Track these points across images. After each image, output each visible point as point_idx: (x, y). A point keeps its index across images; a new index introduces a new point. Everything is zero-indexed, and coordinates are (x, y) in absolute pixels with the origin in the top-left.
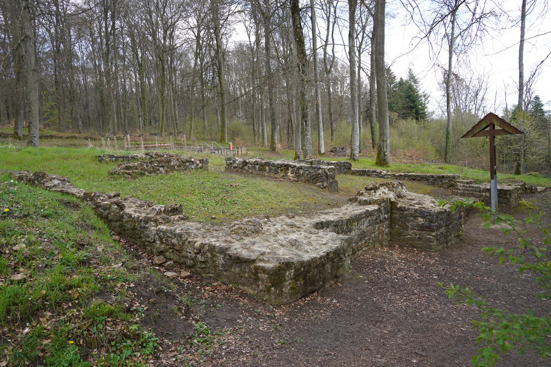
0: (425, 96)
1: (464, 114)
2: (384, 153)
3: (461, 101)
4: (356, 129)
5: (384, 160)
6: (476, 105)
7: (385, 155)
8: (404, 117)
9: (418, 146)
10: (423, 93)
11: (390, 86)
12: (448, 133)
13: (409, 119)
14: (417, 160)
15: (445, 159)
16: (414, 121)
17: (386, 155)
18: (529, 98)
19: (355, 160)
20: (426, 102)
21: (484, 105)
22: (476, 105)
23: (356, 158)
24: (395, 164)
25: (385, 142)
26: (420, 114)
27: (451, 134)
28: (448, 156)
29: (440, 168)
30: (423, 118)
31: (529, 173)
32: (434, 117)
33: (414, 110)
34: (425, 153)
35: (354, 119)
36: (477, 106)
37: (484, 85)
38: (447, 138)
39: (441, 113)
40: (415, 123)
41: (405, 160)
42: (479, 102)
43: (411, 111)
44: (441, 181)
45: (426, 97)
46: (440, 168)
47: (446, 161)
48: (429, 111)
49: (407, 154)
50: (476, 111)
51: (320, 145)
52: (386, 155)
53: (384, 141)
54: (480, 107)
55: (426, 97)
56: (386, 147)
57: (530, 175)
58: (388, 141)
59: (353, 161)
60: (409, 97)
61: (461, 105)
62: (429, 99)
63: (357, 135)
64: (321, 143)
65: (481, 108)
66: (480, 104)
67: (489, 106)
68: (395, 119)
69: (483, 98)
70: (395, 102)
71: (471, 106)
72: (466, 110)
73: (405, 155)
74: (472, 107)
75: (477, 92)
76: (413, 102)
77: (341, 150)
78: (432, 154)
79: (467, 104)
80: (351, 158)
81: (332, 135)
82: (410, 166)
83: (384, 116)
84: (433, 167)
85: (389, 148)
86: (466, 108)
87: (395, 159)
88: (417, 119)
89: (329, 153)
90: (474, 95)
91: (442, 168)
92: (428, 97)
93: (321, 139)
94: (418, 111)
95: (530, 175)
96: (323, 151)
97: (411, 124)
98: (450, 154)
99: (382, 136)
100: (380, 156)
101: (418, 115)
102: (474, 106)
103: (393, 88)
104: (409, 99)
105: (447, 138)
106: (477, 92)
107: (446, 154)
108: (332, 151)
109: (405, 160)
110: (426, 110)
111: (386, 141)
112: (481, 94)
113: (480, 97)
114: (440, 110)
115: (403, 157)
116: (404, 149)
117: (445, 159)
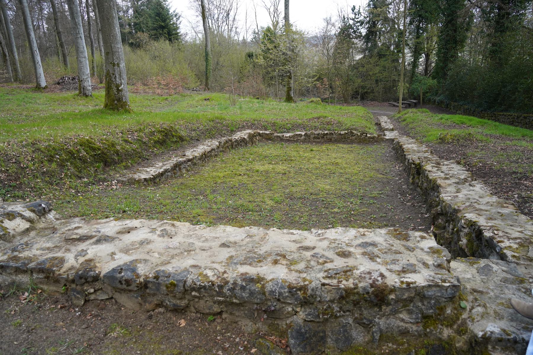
0: (176, 15)
1: (217, 36)
2: (118, 86)
3: (213, 22)
4: (82, 49)
5: (119, 100)
6: (228, 25)
7: (119, 91)
8: (156, 38)
9: (174, 71)
10: (174, 12)
11: (138, 4)
12: (207, 55)
13: (162, 40)
14: (175, 89)
15: (207, 84)
16: (167, 42)
17: (121, 91)
18: (277, 18)
19: (87, 96)
20: (178, 22)
21: (236, 25)
22: (228, 25)
23: (87, 92)
24: (146, 97)
25: (116, 67)
26: (173, 34)
27: (211, 56)
28: (209, 81)
29: (205, 100)
30: (177, 39)
31: (311, 100)
32: (188, 39)
33: (165, 31)
34: (183, 79)
35: (76, 34)
36: (229, 27)
37: (234, 5)
38: (207, 60)
39: (194, 34)
40: (168, 45)
41: (159, 91)
42: (231, 22)
43: (163, 31)
44: (367, 326)
45: (177, 17)
46: (205, 100)
47: (207, 87)
48: (182, 32)
49: (163, 82)
50: (228, 32)
51: (38, 75)
52: (121, 91)
53: (114, 65)
54: (232, 28)
55: (177, 17)
56: (120, 76)
57: (311, 102)
58: (123, 65)
59: (84, 98)
60: (159, 14)
61: (214, 25)
62: (181, 19)
63: (85, 57)
64: (38, 73)
65: (234, 29)
66: (232, 25)
67: (240, 27)
68: (145, 41)
69: (234, 18)
70: (145, 22)
71: (223, 27)
72: (219, 32)
73: (159, 84)
74: (225, 27)
75: (229, 11)
76: (164, 21)
77: (71, 82)
78: (193, 82)
79: (219, 25)
80: (80, 93)
81: (65, 61)
82: (166, 99)
83: (108, 19)
84: (197, 99)
85: (125, 76)
86: (219, 28)
87: (147, 90)
88: (170, 40)
89: (54, 86)
90: (225, 15)
91: (208, 99)
92: (180, 17)
93: (38, 66)
94: (170, 31)
95: (311, 102)
96: (43, 84)
97: (163, 45)
98: (211, 79)
99: (110, 56)
100: (111, 93)
101: (171, 35)
102: (227, 27)
103: (140, 7)
104: (159, 17)
105: (207, 60)
106: (229, 11)
107: (207, 79)
108: (59, 83)
109: (159, 91)
110: (178, 31)
111: (118, 65)
112: (232, 14)
113: (231, 18)
114: (193, 31)
115: (156, 86)
116: (157, 75)
117: (207, 84)
